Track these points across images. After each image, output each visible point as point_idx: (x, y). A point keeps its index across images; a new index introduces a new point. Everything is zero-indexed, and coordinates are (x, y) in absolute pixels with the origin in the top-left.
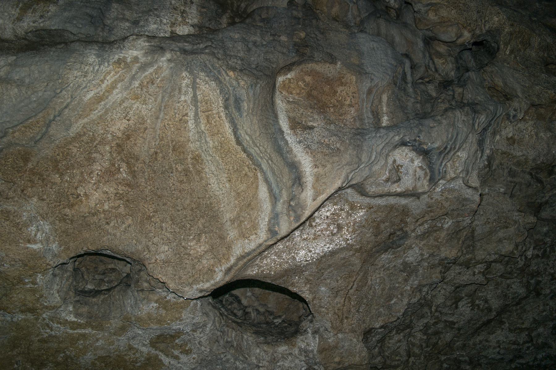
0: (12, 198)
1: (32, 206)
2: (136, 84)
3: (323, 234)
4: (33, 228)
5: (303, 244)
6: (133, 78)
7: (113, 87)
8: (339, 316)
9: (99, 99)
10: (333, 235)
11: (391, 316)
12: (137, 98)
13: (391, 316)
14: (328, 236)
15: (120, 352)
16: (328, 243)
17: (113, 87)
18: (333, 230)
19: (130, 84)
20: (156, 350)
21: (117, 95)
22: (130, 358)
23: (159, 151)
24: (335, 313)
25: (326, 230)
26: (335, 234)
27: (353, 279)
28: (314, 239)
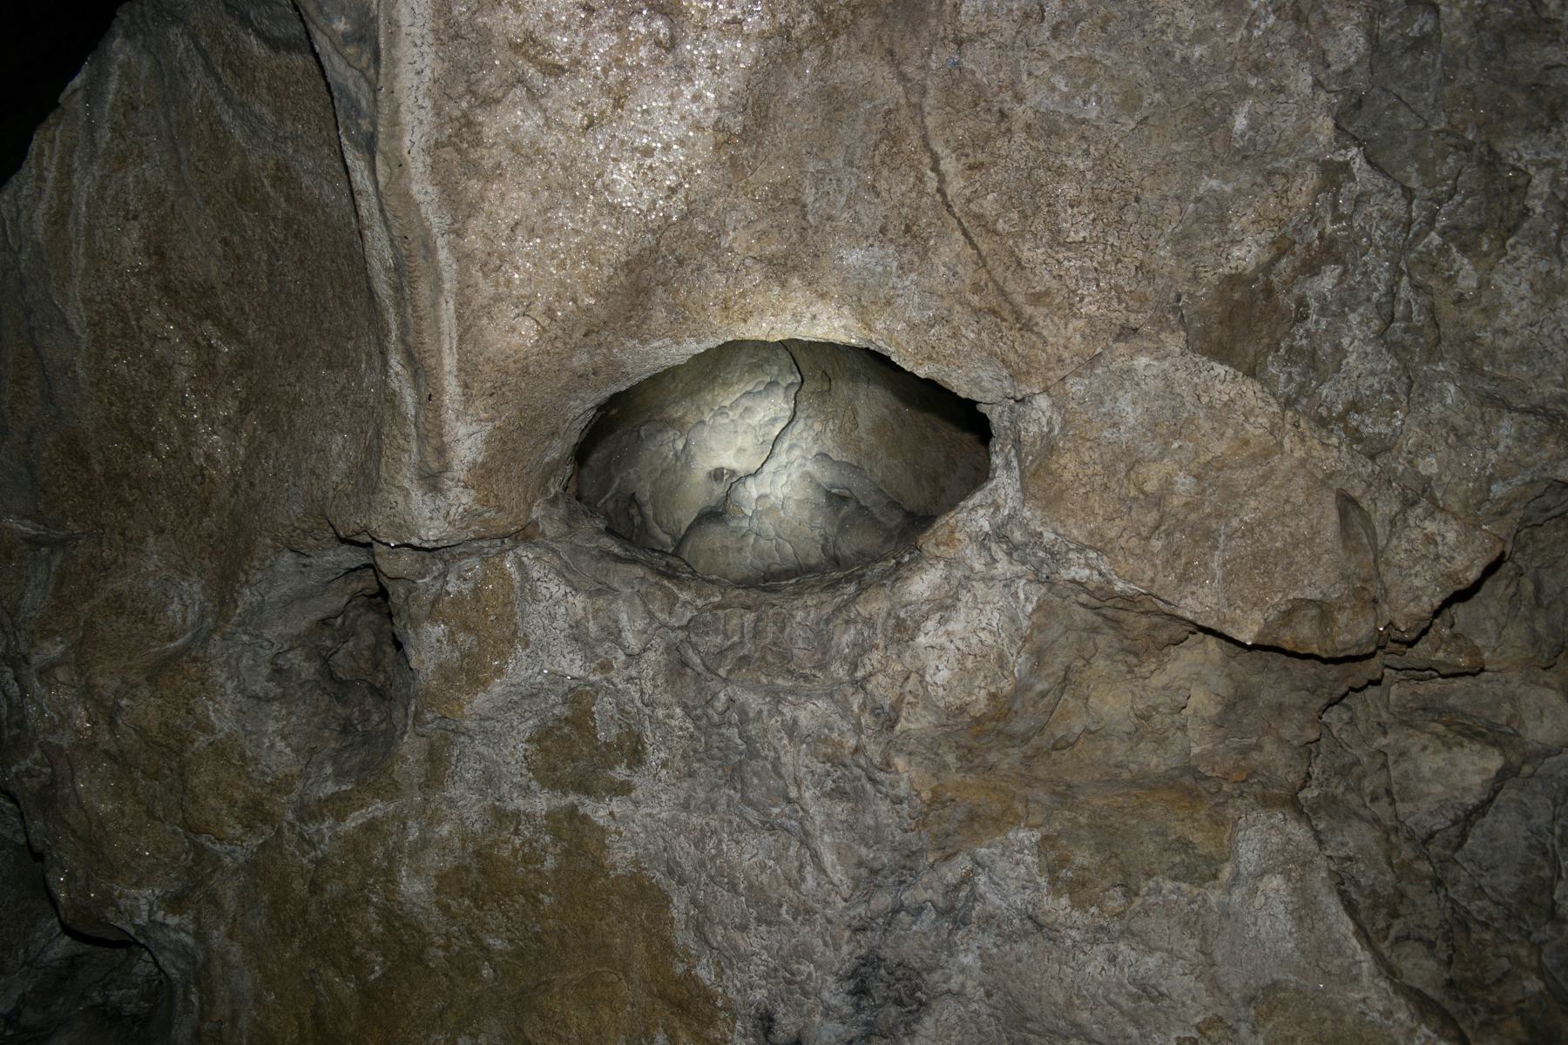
0: (115, 560)
1: (154, 557)
2: (105, 135)
3: (631, 68)
4: (176, 606)
5: (597, 144)
6: (91, 128)
7: (66, 172)
8: (994, 313)
9: (59, 218)
10: (672, 45)
11: (1279, 182)
12: (122, 160)
13: (1279, 182)
14: (656, 61)
15: (474, 840)
16: (677, 82)
17: (66, 172)
18: (653, 35)
19: (93, 142)
20: (565, 794)
21: (84, 186)
22: (515, 851)
23: (226, 234)
24: (976, 311)
25: (626, 45)
26: (672, 38)
27: (914, 139)
28: (618, 104)
